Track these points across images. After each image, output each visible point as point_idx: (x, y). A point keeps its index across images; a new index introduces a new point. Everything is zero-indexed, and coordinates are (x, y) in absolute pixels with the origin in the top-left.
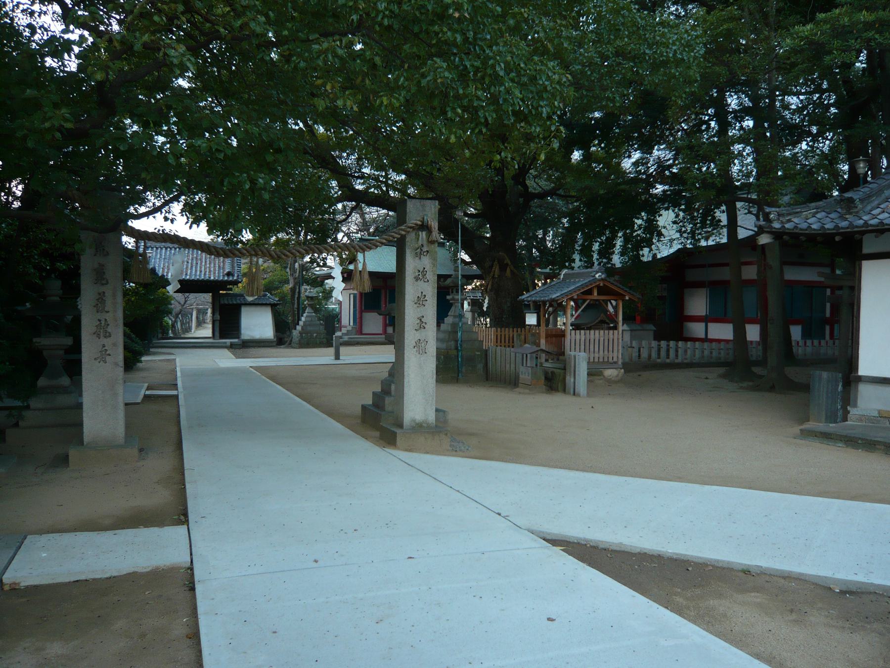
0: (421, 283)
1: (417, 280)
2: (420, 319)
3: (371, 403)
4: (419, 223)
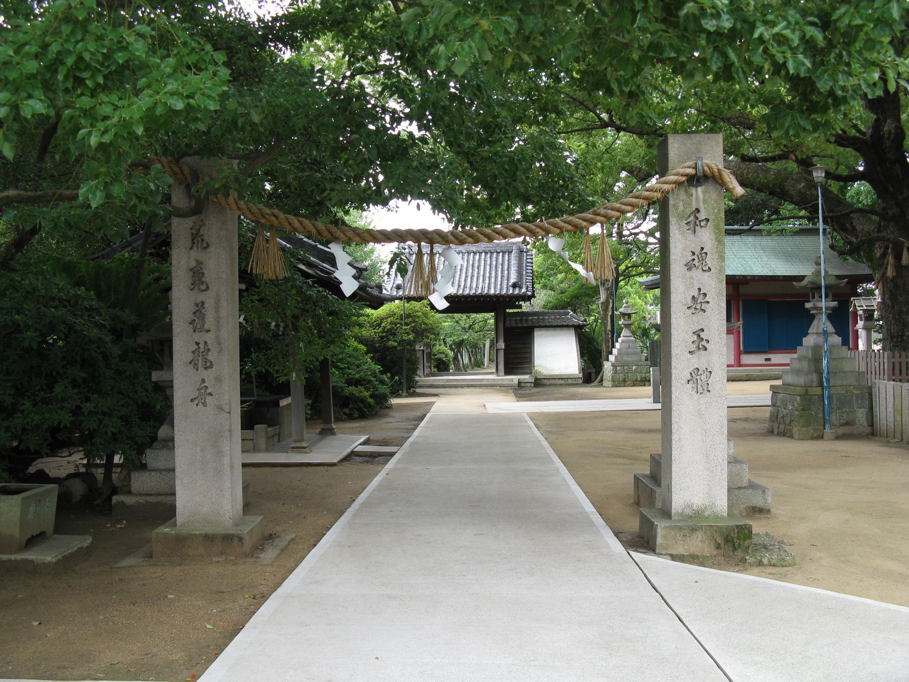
0: (697, 273)
1: (690, 269)
2: (698, 333)
3: (649, 472)
4: (691, 171)
